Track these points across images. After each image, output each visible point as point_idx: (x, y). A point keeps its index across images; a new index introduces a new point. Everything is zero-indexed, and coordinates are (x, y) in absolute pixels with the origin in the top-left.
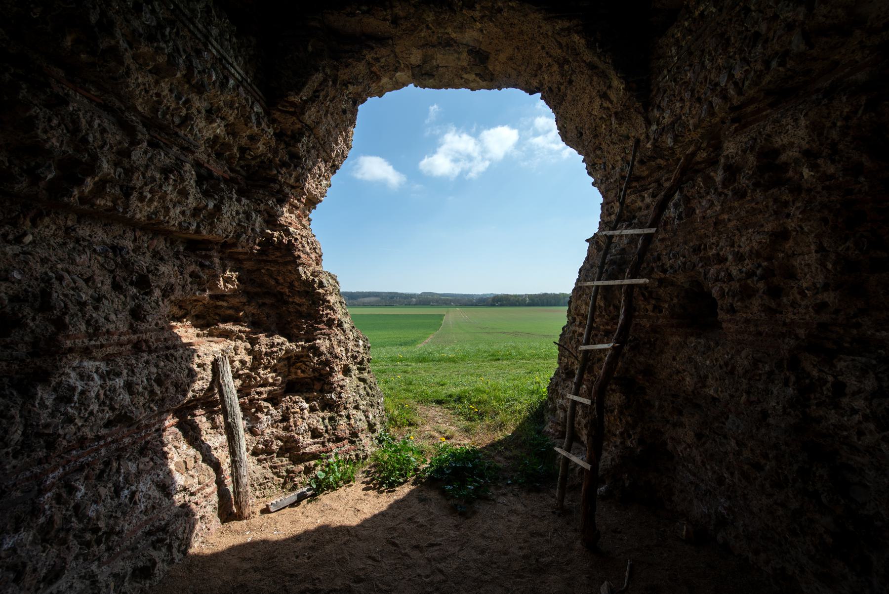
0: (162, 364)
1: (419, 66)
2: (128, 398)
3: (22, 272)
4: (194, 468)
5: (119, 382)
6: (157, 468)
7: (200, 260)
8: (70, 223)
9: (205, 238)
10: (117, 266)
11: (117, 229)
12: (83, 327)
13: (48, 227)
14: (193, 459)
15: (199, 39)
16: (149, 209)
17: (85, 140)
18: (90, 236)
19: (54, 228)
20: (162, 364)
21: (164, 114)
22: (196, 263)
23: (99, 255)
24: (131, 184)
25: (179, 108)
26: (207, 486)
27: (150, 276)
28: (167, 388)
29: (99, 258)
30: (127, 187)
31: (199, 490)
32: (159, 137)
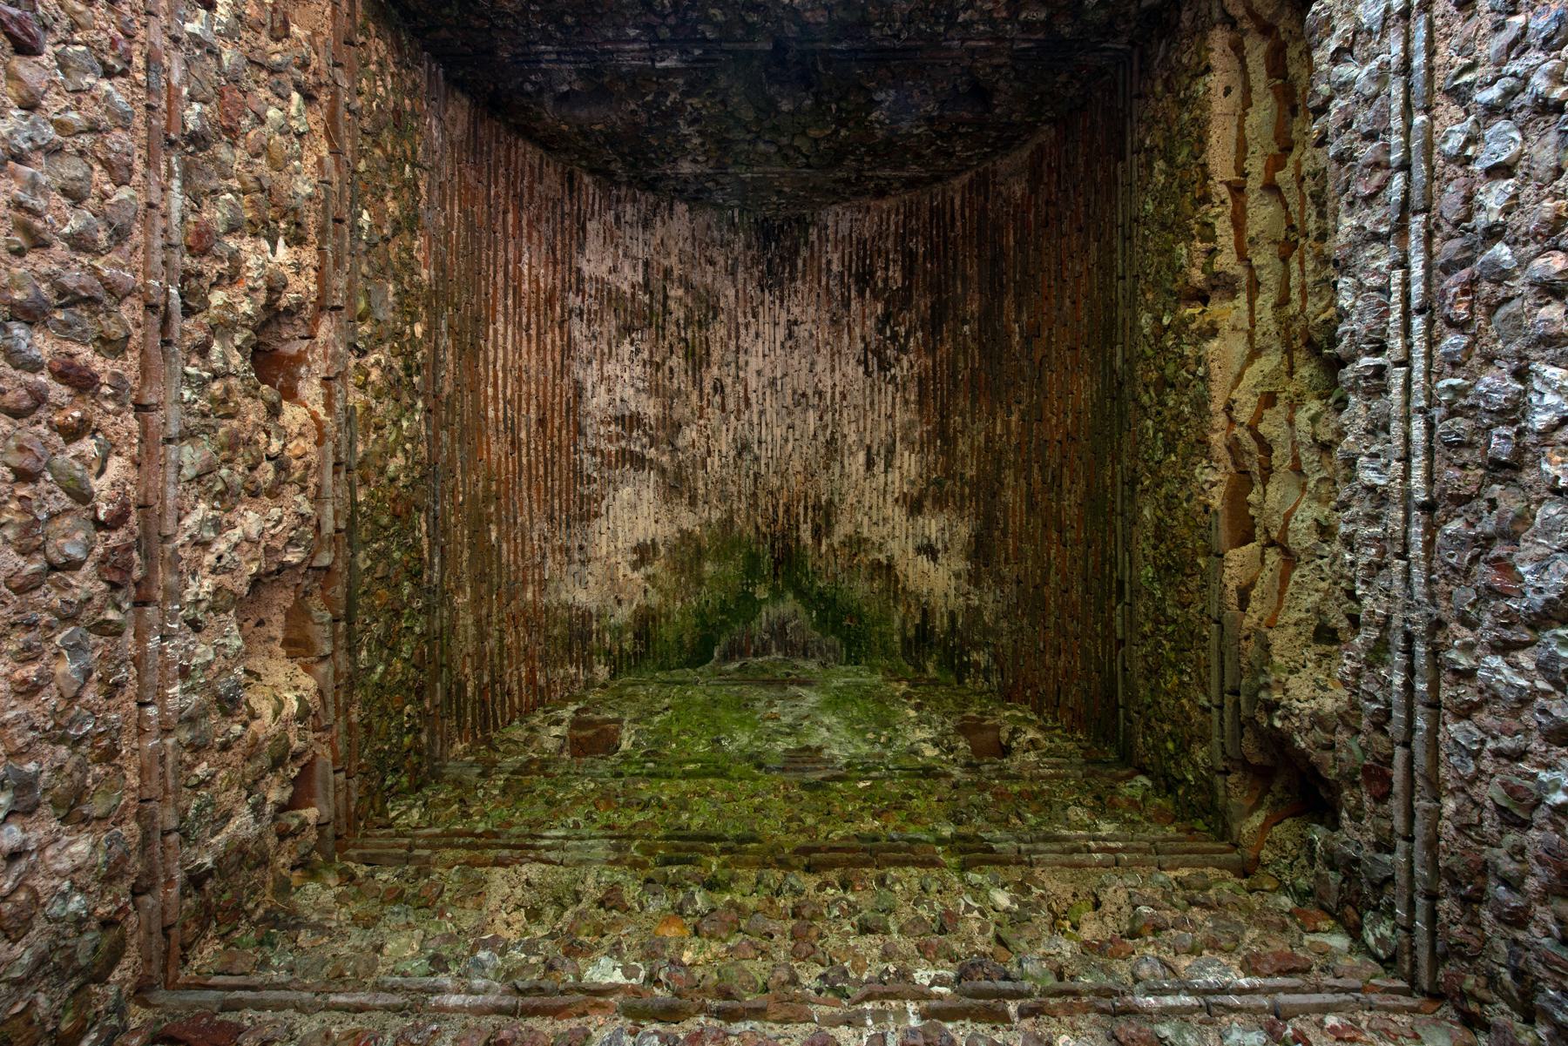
1: (1540, 502)
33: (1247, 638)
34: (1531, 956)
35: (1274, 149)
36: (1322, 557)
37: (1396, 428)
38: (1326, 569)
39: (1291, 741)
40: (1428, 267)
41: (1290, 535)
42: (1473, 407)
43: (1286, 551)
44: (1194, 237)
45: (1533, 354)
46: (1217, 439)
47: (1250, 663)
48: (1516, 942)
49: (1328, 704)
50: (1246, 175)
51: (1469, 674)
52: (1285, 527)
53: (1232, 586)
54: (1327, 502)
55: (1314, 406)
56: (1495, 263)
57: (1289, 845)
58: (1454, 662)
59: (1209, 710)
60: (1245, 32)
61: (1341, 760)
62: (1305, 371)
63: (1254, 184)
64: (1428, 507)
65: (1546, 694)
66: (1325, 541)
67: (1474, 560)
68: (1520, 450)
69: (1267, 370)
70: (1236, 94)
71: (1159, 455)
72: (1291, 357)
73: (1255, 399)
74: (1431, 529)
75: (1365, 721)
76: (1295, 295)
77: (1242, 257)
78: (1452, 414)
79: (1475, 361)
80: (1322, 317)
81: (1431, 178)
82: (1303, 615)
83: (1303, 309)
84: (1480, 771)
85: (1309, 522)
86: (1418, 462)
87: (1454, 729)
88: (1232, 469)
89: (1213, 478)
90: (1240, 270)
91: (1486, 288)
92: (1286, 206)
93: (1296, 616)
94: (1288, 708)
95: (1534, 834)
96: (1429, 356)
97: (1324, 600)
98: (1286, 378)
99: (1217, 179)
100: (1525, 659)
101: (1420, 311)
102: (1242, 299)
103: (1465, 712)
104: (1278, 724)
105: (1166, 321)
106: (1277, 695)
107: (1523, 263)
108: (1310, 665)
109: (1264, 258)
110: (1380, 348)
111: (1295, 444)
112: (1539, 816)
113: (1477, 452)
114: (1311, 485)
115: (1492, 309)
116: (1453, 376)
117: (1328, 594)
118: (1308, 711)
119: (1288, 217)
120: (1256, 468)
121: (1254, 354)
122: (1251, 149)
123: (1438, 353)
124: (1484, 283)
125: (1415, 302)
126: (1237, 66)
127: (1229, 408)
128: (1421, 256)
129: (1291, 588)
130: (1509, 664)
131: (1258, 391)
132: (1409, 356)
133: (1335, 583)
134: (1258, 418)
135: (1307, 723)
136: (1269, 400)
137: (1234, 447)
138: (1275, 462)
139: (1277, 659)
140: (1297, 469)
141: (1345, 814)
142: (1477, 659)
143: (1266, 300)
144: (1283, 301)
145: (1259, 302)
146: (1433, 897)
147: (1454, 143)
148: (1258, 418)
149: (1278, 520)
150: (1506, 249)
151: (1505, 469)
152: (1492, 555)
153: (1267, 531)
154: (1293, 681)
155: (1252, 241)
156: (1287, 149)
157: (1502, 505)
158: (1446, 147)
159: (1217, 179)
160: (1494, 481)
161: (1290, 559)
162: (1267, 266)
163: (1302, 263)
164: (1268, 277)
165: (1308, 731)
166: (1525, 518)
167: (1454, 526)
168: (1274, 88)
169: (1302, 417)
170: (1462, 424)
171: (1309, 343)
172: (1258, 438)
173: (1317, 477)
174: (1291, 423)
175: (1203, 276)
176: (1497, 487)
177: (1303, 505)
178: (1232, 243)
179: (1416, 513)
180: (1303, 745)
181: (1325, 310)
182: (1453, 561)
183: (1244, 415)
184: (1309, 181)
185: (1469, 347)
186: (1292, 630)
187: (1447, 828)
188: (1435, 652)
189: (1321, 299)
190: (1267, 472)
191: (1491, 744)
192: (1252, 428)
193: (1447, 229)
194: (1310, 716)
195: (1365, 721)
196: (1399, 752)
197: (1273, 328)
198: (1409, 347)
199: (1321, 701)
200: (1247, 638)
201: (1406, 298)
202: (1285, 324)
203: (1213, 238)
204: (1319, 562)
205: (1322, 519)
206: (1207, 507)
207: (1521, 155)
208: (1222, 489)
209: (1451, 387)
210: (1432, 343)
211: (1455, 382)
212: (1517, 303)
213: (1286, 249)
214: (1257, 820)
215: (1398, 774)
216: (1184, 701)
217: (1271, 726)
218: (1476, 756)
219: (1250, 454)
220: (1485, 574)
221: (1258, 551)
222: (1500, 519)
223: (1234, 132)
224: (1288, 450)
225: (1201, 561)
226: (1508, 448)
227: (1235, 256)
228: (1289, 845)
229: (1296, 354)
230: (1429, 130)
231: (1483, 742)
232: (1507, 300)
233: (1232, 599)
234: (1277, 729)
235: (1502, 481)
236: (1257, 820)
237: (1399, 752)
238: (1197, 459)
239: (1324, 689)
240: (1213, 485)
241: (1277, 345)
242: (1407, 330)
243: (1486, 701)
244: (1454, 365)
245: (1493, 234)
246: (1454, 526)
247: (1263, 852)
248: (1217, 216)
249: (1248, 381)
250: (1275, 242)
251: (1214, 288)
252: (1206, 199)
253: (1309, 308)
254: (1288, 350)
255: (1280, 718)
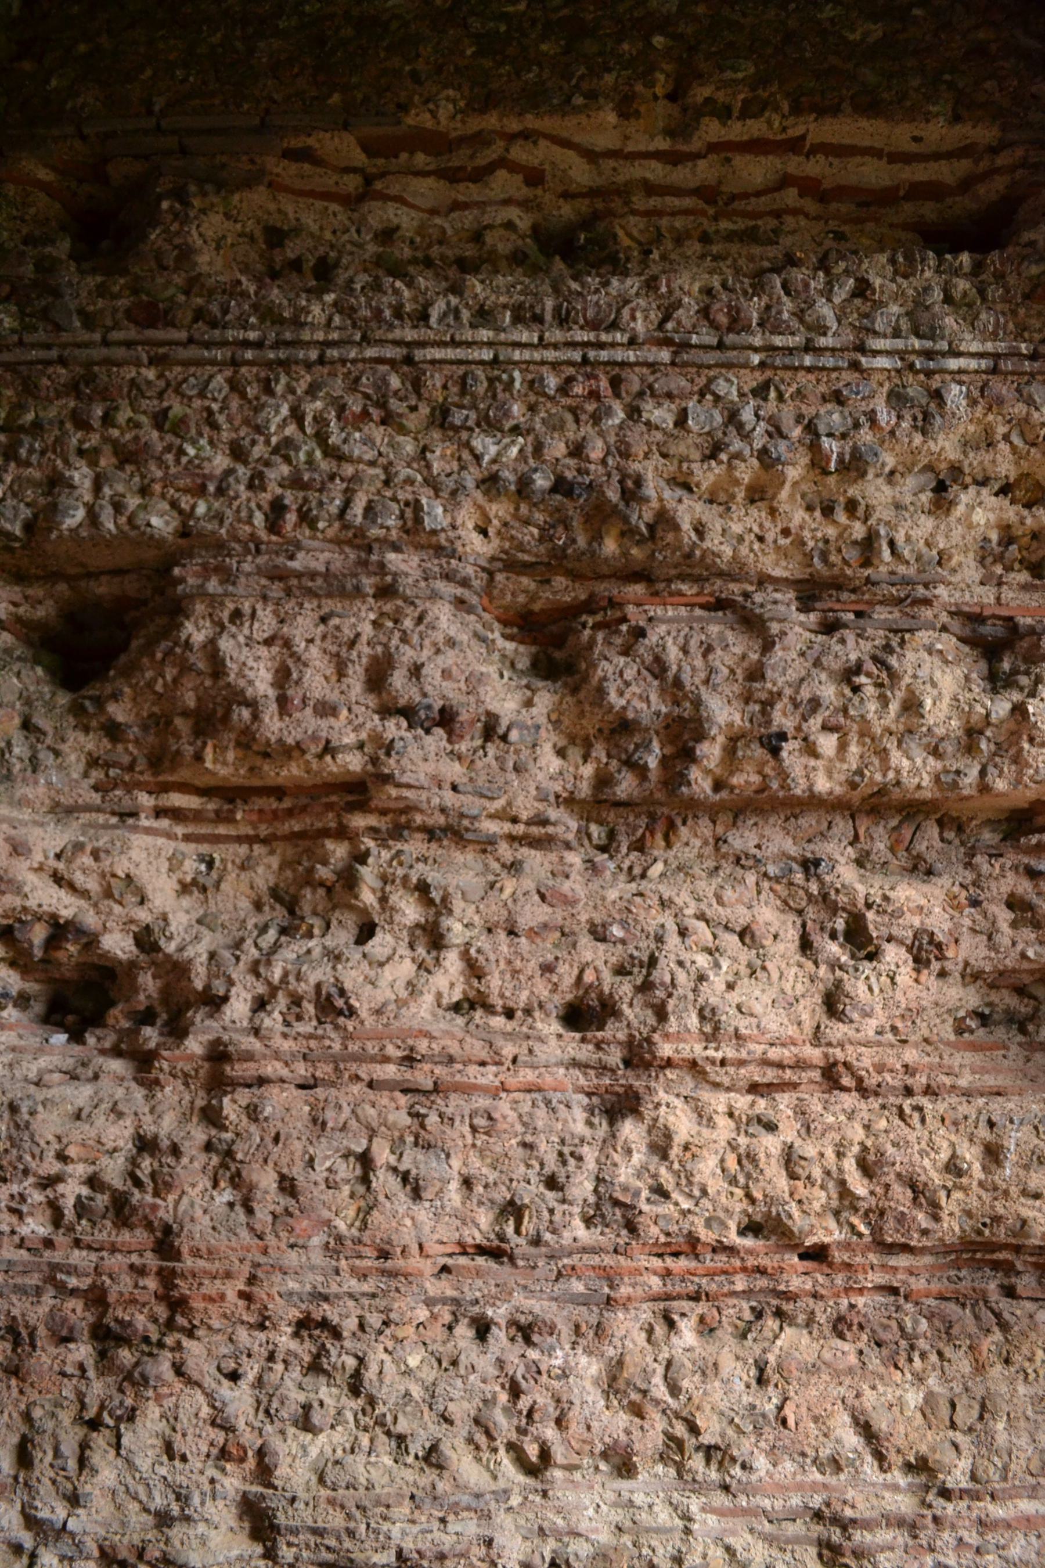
0: (883, 1124)
1: (416, 439)
2: (782, 1183)
3: (624, 924)
4: (971, 1430)
5: (770, 1144)
6: (863, 1378)
7: (1026, 860)
8: (720, 830)
9: (1006, 804)
10: (810, 901)
11: (808, 822)
12: (693, 1021)
13: (687, 844)
14: (977, 1407)
15: (835, 369)
16: (845, 767)
17: (678, 683)
18: (758, 847)
19: (698, 843)
20: (883, 1124)
21: (824, 556)
22: (1017, 872)
23: (778, 882)
24: (774, 729)
25: (846, 528)
26: (993, 1497)
27: (870, 915)
28: (887, 1187)
29: (778, 887)
30: (770, 736)
31: (963, 1493)
32: (837, 606)
33: (252, 161)
34: (57, 432)
35: (826, 185)
36: (358, 231)
37: (485, 334)
38: (346, 237)
39: (154, 223)
40: (623, 364)
41: (379, 204)
42: (494, 397)
43: (361, 198)
44: (753, 89)
45: (530, 438)
46: (492, 121)
47: (223, 166)
48: (62, 423)
49: (205, 260)
50: (807, 157)
51: (269, 391)
52: (386, 198)
53: (311, 141)
54: (418, 233)
55: (524, 222)
56: (609, 412)
57: (32, 211)
58: (277, 381)
59: (150, 113)
60: (976, 162)
61: (153, 279)
62: (567, 211)
63: (795, 165)
64: (409, 360)
65: (267, 442)
66: (376, 236)
67: (367, 396)
68: (456, 429)
69: (571, 173)
70: (914, 148)
71: (475, 24)
72: (583, 195)
73: (536, 162)
74: (392, 362)
75: (199, 301)
76: (654, 202)
77: (713, 148)
78: (491, 381)
79: (532, 398)
80: (621, 233)
81: (700, 366)
82: (291, 215)
83: (634, 212)
84: (190, 398)
85: (396, 221)
86: (450, 353)
87: (219, 380)
88: (454, 134)
89: (443, 115)
90: (696, 145)
91: (591, 407)
92: (758, 194)
93: (290, 209)
94: (185, 220)
95: (155, 434)
96: (543, 363)
97: (312, 235)
98: (560, 189)
99: (812, 127)
100: (291, 430)
101: (585, 359)
102: (662, 144)
103: (235, 386)
104: (165, 205)
105: (658, 40)
106: (196, 202)
107: (601, 434)
108: (239, 226)
109: (705, 171)
110: (563, 320)
111: (482, 205)
112: (169, 438)
113: (456, 399)
114: (438, 221)
115: (574, 411)
116: (523, 381)
117: (318, 239)
118: (190, 240)
119: (746, 196)
120: (455, 163)
121: (591, 155)
122: (836, 161)
123: (545, 370)
124: (595, 406)
125: (592, 354)
126: (945, 148)
127: (526, 135)
128: (632, 359)
129: (319, 204)
130: (284, 420)
131: (547, 167)
132: (546, 347)
133: (332, 247)
134: (514, 167)
135: (177, 241)
136: (534, 177)
137: (480, 140)
138: (461, 187)
139: (237, 197)
140: (457, 206)
141: (99, 279)
142: (283, 396)
143: (655, 171)
144: (650, 189)
145: (654, 164)
146: (62, 361)
147: (721, 387)
148: (514, 167)
149: (394, 190)
150: (617, 421)
151: (441, 417)
152: (371, 410)
153: (383, 175)
154: (216, 219)
155: (728, 160)
156: (823, 197)
157: (413, 416)
158: (721, 381)
159: (812, 127)
160: (433, 409)
161: (352, 202)
162: (694, 174)
163: (686, 212)
164: (681, 176)
165: (169, 241)
166: (402, 430)
167: (395, 382)
168: (897, 188)
169: (513, 213)
170: (481, 388)
171: (597, 215)
172: (491, 168)
173: (447, 225)
174: (507, 202)
175: (700, 99)
176: (427, 411)
177: (413, 213)
178: (732, 137)
179: (405, 351)
180: (153, 237)
181: (629, 235)
182: (364, 380)
183: (519, 153)
184: (772, 223)
185: (545, 395)
186: (272, 207)
187: (130, 373)
188: (285, 364)
189: (641, 231)
190: (451, 176)
191: (215, 407)
192: (502, 163)
193: (651, 379)
194: (186, 244)
195: (199, 301)
196: (183, 335)
197: (620, 179)
198: (555, 346)
199: (205, 249)
200: (252, 161)
201: (601, 346)
202: (623, 191)
203: (744, 115)
204: (353, 229)
205: (399, 233)
206: (403, 108)
207: (689, 432)
208: (429, 124)
209: (512, 380)
210: (555, 365)
211: (517, 385)
212: (574, 426)
213: (707, 193)
214: (44, 174)
215: (159, 334)
216: (149, 72)
217: (160, 198)
218: (202, 395)
219: (472, 157)
220: (355, 406)
221: (358, 164)
222: (401, 415)
223: (867, 143)
224: (476, 198)
225: (336, 98)
226: (458, 422)
227: (715, 140)
228: (32, 211)
229: (587, 201)
230: (746, 365)
231: (215, 400)
232: (577, 421)
233: (296, 143)
234: (159, 204)
235: (432, 413)
236: (44, 174)
237: (183, 335)
238: (467, 93)
239: (218, 248)
240: (434, 116)
241: (600, 181)
242: (573, 345)
243: (250, 402)
244: (532, 383)
245: (634, 412)
246: (395, 382)
247: (12, 187)
248: (769, 123)
249: (557, 152)
250: (720, 183)
251: (684, 110)
252: (797, 110)
253: (632, 219)
254: (593, 193)
255: (171, 207)
